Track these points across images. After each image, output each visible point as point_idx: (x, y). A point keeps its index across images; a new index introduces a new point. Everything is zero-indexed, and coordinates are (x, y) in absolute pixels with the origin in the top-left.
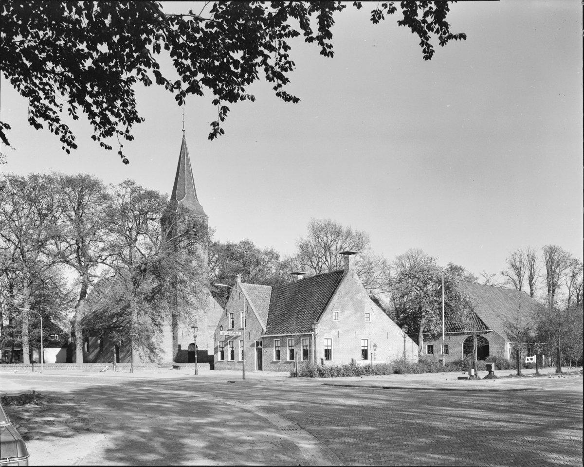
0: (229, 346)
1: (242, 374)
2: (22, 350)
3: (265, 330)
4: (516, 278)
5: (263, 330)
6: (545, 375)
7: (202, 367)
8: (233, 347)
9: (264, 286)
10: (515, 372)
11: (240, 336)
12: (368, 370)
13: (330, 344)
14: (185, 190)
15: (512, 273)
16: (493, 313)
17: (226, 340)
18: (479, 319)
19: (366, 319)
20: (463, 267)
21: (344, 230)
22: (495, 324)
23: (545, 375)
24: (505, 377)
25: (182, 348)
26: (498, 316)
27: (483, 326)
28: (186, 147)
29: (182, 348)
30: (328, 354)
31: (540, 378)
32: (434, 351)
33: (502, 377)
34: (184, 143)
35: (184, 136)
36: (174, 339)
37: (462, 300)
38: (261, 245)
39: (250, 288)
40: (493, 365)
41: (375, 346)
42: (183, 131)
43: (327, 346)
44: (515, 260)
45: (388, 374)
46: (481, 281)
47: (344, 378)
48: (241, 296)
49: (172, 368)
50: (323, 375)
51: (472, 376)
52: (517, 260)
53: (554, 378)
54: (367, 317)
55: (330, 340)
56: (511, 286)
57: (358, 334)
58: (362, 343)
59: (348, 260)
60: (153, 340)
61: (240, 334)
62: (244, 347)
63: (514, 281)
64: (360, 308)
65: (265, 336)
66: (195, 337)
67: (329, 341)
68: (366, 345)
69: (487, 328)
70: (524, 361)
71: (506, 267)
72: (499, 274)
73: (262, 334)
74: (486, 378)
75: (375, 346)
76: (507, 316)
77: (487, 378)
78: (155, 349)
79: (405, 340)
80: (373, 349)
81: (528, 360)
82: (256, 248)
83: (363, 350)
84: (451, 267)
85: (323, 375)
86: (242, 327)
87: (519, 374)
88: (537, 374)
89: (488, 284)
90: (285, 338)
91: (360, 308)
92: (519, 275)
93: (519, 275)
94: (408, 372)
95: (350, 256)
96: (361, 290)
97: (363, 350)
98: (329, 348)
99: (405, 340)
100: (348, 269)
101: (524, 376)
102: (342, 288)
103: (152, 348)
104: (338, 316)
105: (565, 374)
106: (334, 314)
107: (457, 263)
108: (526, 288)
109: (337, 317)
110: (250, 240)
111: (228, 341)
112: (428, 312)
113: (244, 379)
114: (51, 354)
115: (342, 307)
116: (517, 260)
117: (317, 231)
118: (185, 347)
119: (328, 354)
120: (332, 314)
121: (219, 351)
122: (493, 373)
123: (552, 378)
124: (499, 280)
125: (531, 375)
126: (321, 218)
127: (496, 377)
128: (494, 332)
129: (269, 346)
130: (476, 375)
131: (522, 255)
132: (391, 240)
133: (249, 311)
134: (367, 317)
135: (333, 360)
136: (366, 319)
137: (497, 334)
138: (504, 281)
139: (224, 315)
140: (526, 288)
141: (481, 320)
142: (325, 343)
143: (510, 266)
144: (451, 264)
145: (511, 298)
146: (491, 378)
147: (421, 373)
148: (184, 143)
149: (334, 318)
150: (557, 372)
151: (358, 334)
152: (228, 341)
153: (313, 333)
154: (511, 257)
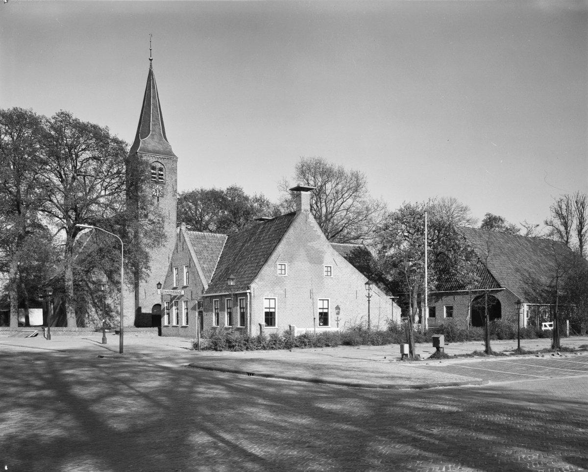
0: (174, 308)
1: (118, 344)
2: (10, 311)
3: (206, 287)
4: (562, 228)
5: (203, 288)
6: (530, 353)
7: (148, 333)
8: (177, 309)
9: (218, 235)
10: (480, 346)
11: (183, 296)
12: (325, 341)
13: (326, 306)
14: (149, 127)
15: (558, 222)
16: (512, 267)
17: (171, 301)
18: (490, 274)
19: (325, 274)
20: (503, 217)
21: (336, 169)
22: (510, 281)
23: (530, 353)
24: (463, 355)
25: (143, 311)
26: (517, 270)
27: (494, 283)
28: (153, 78)
29: (143, 311)
30: (270, 318)
31: (521, 357)
32: (437, 314)
33: (456, 356)
34: (151, 74)
35: (151, 66)
36: (136, 299)
37: (462, 249)
38: (250, 192)
39: (197, 237)
40: (442, 338)
41: (338, 308)
42: (150, 60)
43: (269, 308)
44: (560, 208)
45: (333, 346)
46: (523, 232)
47: (243, 353)
48: (184, 247)
49: (115, 333)
50: (233, 346)
51: (406, 355)
52: (564, 207)
53: (543, 356)
54: (281, 269)
55: (274, 300)
56: (556, 238)
57: (310, 293)
58: (320, 304)
59: (301, 197)
60: (109, 301)
61: (183, 293)
62: (329, 308)
63: (559, 232)
64: (316, 259)
65: (206, 295)
66: (369, 297)
67: (272, 301)
68: (274, 307)
69: (499, 286)
70: (541, 328)
71: (550, 216)
72: (542, 225)
73: (203, 293)
74: (433, 357)
75: (338, 308)
76: (531, 270)
77: (434, 357)
78: (112, 311)
79: (369, 301)
80: (335, 311)
81: (545, 326)
82: (245, 195)
83: (320, 314)
84: (490, 218)
85: (233, 346)
86: (185, 285)
87: (488, 352)
88: (519, 351)
89: (530, 236)
90: (224, 298)
91: (316, 259)
92: (566, 225)
93: (566, 225)
94: (364, 343)
95: (302, 192)
96: (319, 237)
97: (320, 314)
98: (272, 310)
99: (369, 301)
100: (301, 210)
101: (496, 354)
102: (291, 233)
103: (107, 312)
104: (331, 271)
105: (566, 350)
106: (279, 267)
107: (496, 213)
108: (574, 241)
109: (329, 273)
110: (238, 185)
111: (173, 302)
112: (420, 265)
113: (121, 351)
114: (36, 316)
115: (291, 259)
116: (564, 207)
117: (304, 170)
118: (147, 310)
119: (270, 318)
120: (275, 267)
121: (166, 313)
122: (442, 349)
123: (540, 358)
124: (543, 231)
125: (507, 353)
126: (311, 154)
127: (446, 357)
128: (507, 290)
129: (209, 310)
130: (411, 352)
131: (569, 201)
132: (393, 184)
133: (191, 265)
134: (281, 269)
135: (276, 327)
136: (325, 274)
137: (510, 293)
138: (548, 232)
139: (170, 270)
140: (574, 241)
141: (492, 275)
142: (266, 304)
143: (554, 214)
144: (489, 214)
145: (542, 250)
146: (438, 358)
147: (383, 344)
148: (151, 74)
149: (279, 272)
150: (553, 347)
151: (310, 293)
152: (173, 302)
153: (248, 291)
154: (556, 204)
